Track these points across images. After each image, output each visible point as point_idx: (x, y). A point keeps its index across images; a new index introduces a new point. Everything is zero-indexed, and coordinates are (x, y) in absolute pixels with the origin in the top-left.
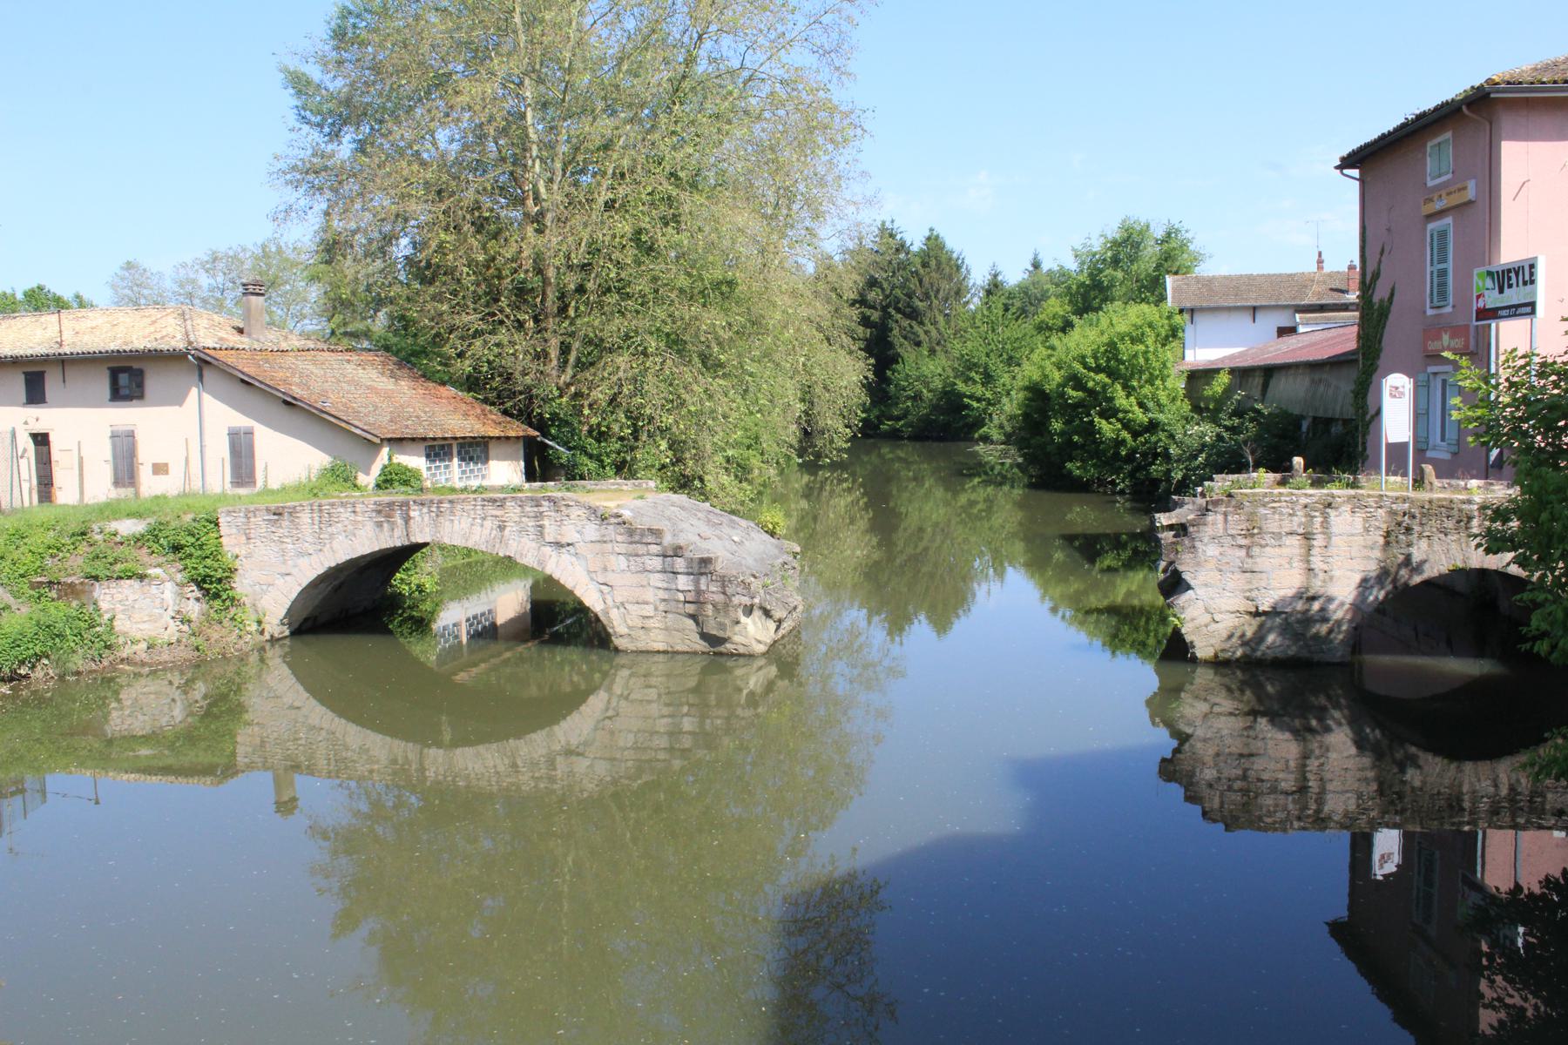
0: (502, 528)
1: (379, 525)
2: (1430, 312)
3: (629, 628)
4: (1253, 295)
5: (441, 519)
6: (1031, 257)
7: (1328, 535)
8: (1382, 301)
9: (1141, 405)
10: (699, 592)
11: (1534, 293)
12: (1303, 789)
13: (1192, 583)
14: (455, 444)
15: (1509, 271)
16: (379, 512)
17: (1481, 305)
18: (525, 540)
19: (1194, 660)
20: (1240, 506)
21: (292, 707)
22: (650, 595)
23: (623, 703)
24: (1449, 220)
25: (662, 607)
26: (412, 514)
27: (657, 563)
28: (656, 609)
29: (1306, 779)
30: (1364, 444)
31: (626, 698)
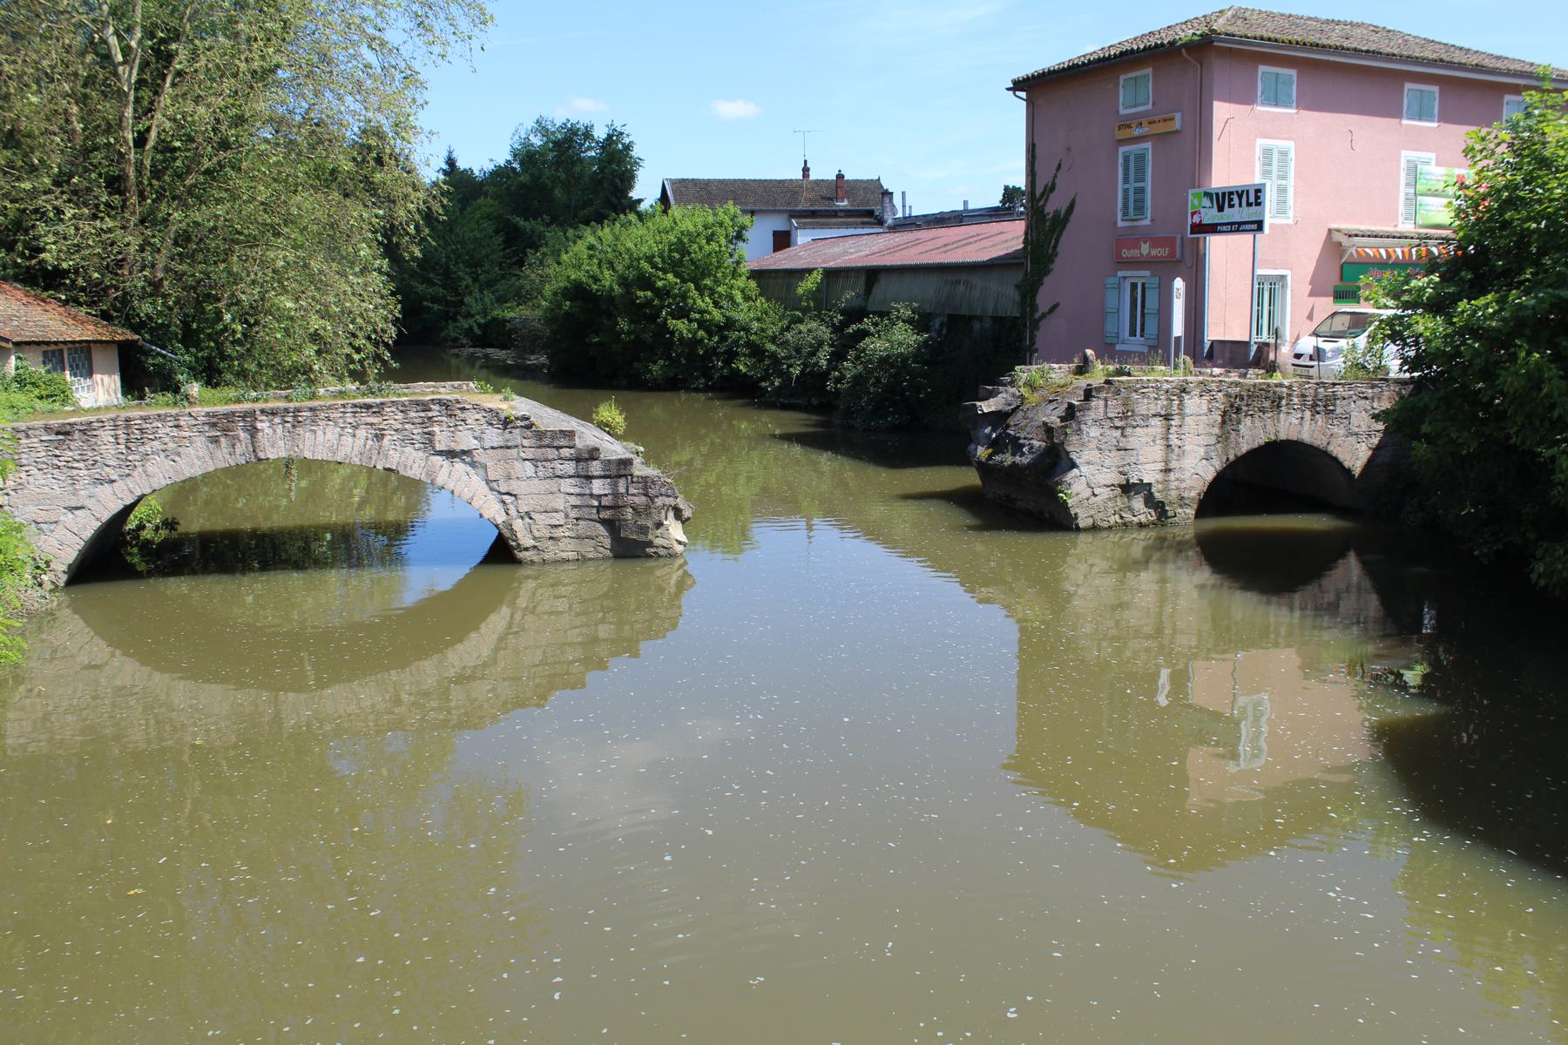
0: (379, 437)
1: (215, 440)
2: (1120, 224)
3: (535, 538)
4: (751, 200)
5: (300, 430)
6: (446, 154)
7: (1182, 415)
8: (1057, 213)
9: (716, 304)
10: (616, 495)
11: (1262, 213)
12: (1159, 631)
13: (1078, 461)
14: (65, 348)
15: (1231, 193)
16: (214, 425)
17: (1196, 219)
18: (409, 449)
19: (1078, 529)
20: (1118, 392)
21: (90, 667)
22: (559, 502)
23: (529, 618)
24: (1148, 145)
25: (574, 514)
26: (259, 425)
27: (570, 468)
28: (567, 516)
29: (1161, 622)
30: (1032, 338)
31: (532, 612)
